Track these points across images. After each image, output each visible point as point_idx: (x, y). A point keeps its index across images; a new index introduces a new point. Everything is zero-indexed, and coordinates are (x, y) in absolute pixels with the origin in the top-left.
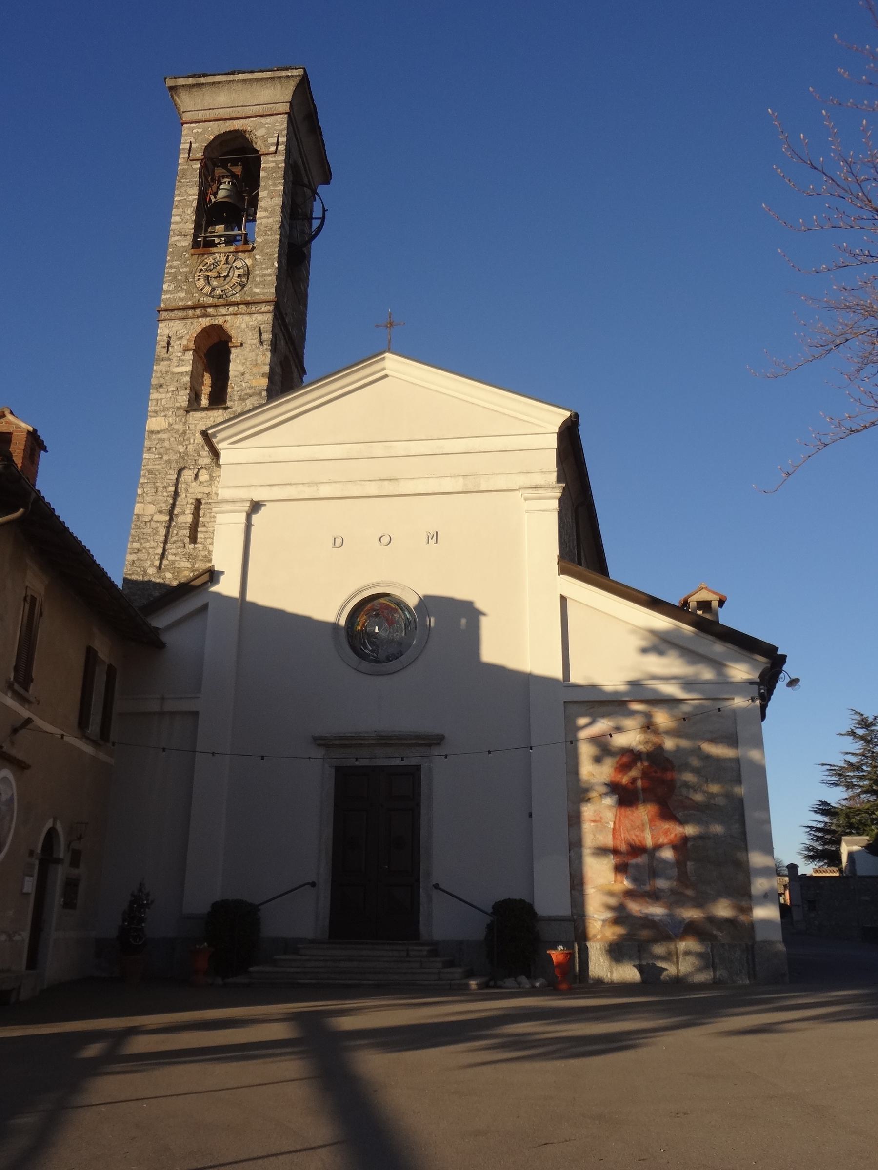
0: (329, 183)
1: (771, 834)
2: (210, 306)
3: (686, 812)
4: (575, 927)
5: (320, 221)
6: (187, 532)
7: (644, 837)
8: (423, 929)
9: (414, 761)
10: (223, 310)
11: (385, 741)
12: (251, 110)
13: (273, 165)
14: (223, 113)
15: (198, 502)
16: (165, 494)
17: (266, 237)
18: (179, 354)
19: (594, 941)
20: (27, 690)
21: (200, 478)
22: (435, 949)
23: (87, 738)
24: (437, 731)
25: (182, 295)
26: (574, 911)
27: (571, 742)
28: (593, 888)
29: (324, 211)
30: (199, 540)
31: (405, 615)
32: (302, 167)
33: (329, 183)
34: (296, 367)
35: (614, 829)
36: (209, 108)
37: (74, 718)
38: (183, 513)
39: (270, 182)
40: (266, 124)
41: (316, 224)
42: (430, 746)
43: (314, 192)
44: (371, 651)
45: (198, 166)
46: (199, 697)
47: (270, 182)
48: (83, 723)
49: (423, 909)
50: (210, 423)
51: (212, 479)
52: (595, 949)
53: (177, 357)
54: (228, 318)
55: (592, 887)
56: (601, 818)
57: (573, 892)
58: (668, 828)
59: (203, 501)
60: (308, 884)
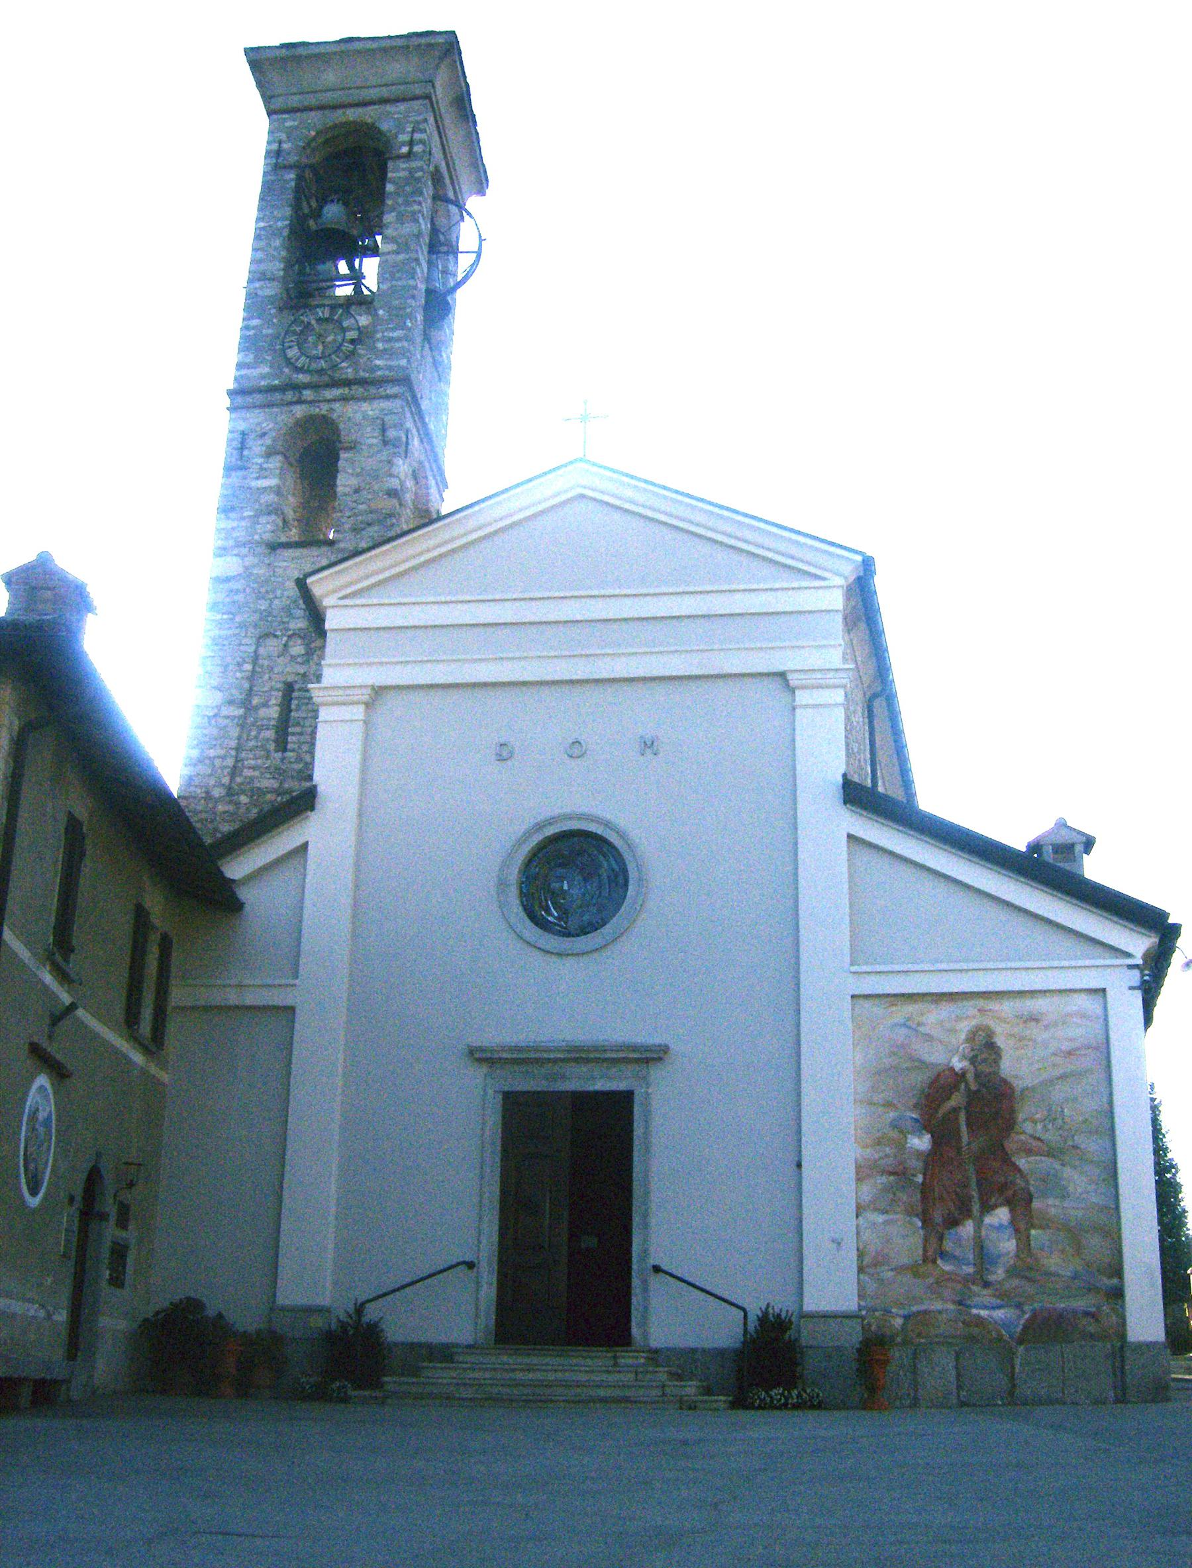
0: (484, 194)
1: (262, 199)
2: (307, 386)
5: (475, 255)
6: (270, 734)
8: (635, 1330)
9: (622, 1086)
10: (329, 394)
11: (581, 1055)
12: (373, 94)
13: (406, 173)
14: (329, 98)
15: (289, 688)
16: (238, 675)
17: (394, 283)
18: (260, 461)
20: (66, 960)
21: (290, 650)
22: (655, 1355)
23: (136, 1039)
24: (656, 1040)
25: (265, 370)
26: (862, 1303)
28: (892, 1270)
29: (481, 240)
30: (290, 746)
31: (609, 865)
32: (446, 174)
33: (484, 194)
34: (435, 478)
37: (119, 1011)
38: (265, 705)
39: (400, 200)
40: (394, 114)
41: (464, 261)
42: (647, 1062)
43: (461, 208)
44: (555, 918)
45: (293, 176)
46: (295, 985)
47: (400, 200)
48: (131, 1019)
49: (636, 1300)
50: (308, 568)
51: (309, 653)
53: (257, 464)
54: (337, 406)
59: (297, 687)
60: (464, 1263)
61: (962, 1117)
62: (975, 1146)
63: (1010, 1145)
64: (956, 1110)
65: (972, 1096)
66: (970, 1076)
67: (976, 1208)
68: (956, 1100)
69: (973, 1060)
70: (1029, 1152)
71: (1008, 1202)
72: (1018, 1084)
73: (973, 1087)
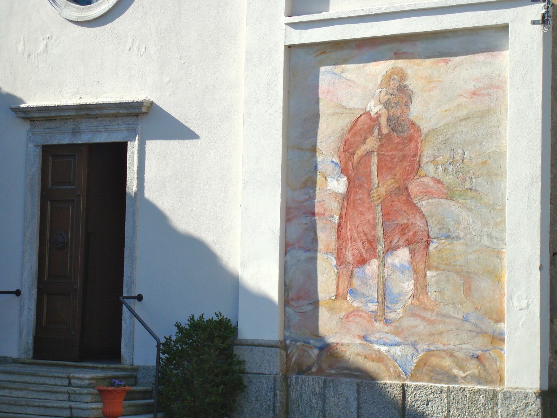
3: (430, 201)
4: (287, 355)
7: (374, 236)
8: (124, 350)
19: (308, 374)
26: (287, 334)
27: (365, 378)
28: (311, 304)
35: (339, 225)
36: (377, 284)
42: (137, 116)
52: (307, 385)
55: (310, 302)
56: (325, 210)
57: (287, 309)
58: (406, 224)
61: (375, 160)
62: (382, 190)
63: (414, 188)
64: (369, 154)
65: (384, 140)
66: (383, 121)
67: (381, 247)
68: (371, 143)
69: (387, 105)
70: (428, 193)
71: (409, 243)
72: (425, 126)
73: (385, 131)
